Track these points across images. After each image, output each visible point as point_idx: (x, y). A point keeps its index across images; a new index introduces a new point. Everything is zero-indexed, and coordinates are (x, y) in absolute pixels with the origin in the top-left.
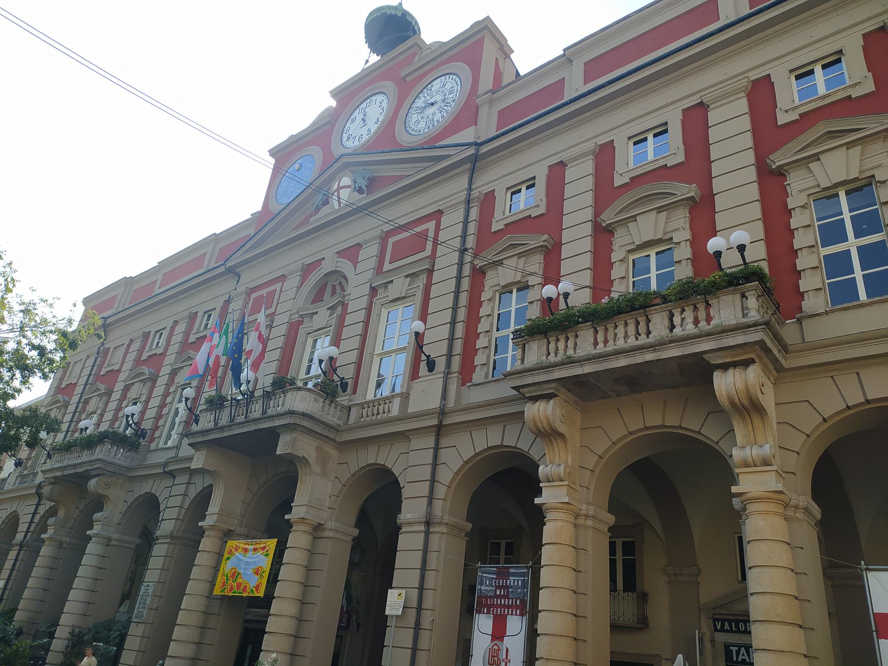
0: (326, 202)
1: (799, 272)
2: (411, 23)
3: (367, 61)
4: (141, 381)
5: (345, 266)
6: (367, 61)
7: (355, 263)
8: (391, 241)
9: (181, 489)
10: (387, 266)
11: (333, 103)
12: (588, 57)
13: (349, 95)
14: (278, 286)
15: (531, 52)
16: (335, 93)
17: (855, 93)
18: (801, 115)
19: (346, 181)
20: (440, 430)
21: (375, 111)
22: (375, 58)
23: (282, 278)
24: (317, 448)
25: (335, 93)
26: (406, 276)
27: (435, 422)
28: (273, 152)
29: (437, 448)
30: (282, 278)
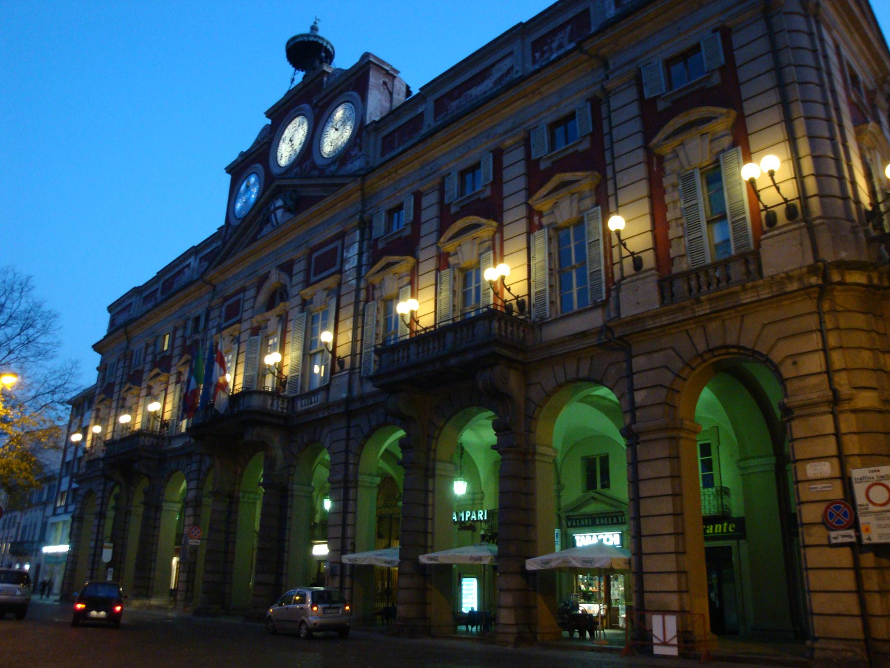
0: (268, 220)
1: (673, 259)
2: (322, 45)
3: (293, 80)
4: (367, 301)
5: (285, 278)
6: (293, 80)
7: (291, 275)
8: (314, 256)
9: (194, 466)
10: (313, 279)
11: (269, 122)
12: (437, 95)
13: (279, 116)
14: (241, 296)
15: (416, 74)
16: (269, 114)
17: (482, 196)
18: (553, 163)
19: (280, 203)
20: (349, 414)
21: (296, 133)
22: (300, 76)
23: (243, 290)
24: (580, 401)
25: (269, 114)
26: (325, 289)
27: (342, 409)
28: (230, 170)
29: (348, 427)
30: (243, 290)
